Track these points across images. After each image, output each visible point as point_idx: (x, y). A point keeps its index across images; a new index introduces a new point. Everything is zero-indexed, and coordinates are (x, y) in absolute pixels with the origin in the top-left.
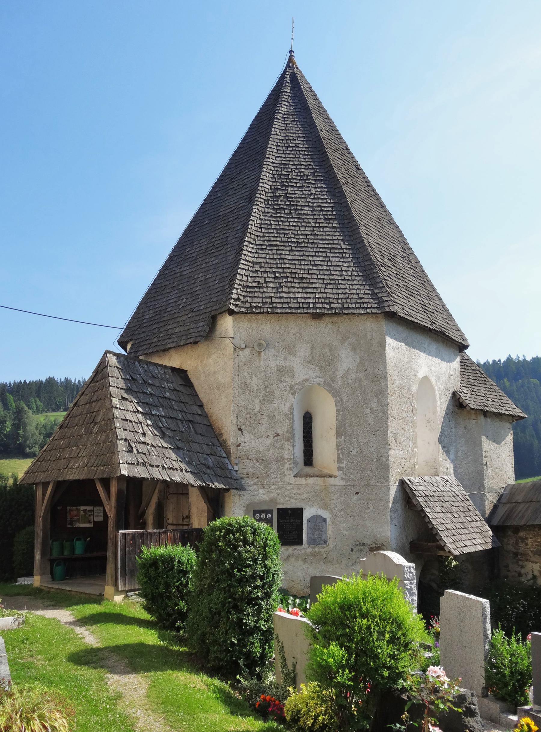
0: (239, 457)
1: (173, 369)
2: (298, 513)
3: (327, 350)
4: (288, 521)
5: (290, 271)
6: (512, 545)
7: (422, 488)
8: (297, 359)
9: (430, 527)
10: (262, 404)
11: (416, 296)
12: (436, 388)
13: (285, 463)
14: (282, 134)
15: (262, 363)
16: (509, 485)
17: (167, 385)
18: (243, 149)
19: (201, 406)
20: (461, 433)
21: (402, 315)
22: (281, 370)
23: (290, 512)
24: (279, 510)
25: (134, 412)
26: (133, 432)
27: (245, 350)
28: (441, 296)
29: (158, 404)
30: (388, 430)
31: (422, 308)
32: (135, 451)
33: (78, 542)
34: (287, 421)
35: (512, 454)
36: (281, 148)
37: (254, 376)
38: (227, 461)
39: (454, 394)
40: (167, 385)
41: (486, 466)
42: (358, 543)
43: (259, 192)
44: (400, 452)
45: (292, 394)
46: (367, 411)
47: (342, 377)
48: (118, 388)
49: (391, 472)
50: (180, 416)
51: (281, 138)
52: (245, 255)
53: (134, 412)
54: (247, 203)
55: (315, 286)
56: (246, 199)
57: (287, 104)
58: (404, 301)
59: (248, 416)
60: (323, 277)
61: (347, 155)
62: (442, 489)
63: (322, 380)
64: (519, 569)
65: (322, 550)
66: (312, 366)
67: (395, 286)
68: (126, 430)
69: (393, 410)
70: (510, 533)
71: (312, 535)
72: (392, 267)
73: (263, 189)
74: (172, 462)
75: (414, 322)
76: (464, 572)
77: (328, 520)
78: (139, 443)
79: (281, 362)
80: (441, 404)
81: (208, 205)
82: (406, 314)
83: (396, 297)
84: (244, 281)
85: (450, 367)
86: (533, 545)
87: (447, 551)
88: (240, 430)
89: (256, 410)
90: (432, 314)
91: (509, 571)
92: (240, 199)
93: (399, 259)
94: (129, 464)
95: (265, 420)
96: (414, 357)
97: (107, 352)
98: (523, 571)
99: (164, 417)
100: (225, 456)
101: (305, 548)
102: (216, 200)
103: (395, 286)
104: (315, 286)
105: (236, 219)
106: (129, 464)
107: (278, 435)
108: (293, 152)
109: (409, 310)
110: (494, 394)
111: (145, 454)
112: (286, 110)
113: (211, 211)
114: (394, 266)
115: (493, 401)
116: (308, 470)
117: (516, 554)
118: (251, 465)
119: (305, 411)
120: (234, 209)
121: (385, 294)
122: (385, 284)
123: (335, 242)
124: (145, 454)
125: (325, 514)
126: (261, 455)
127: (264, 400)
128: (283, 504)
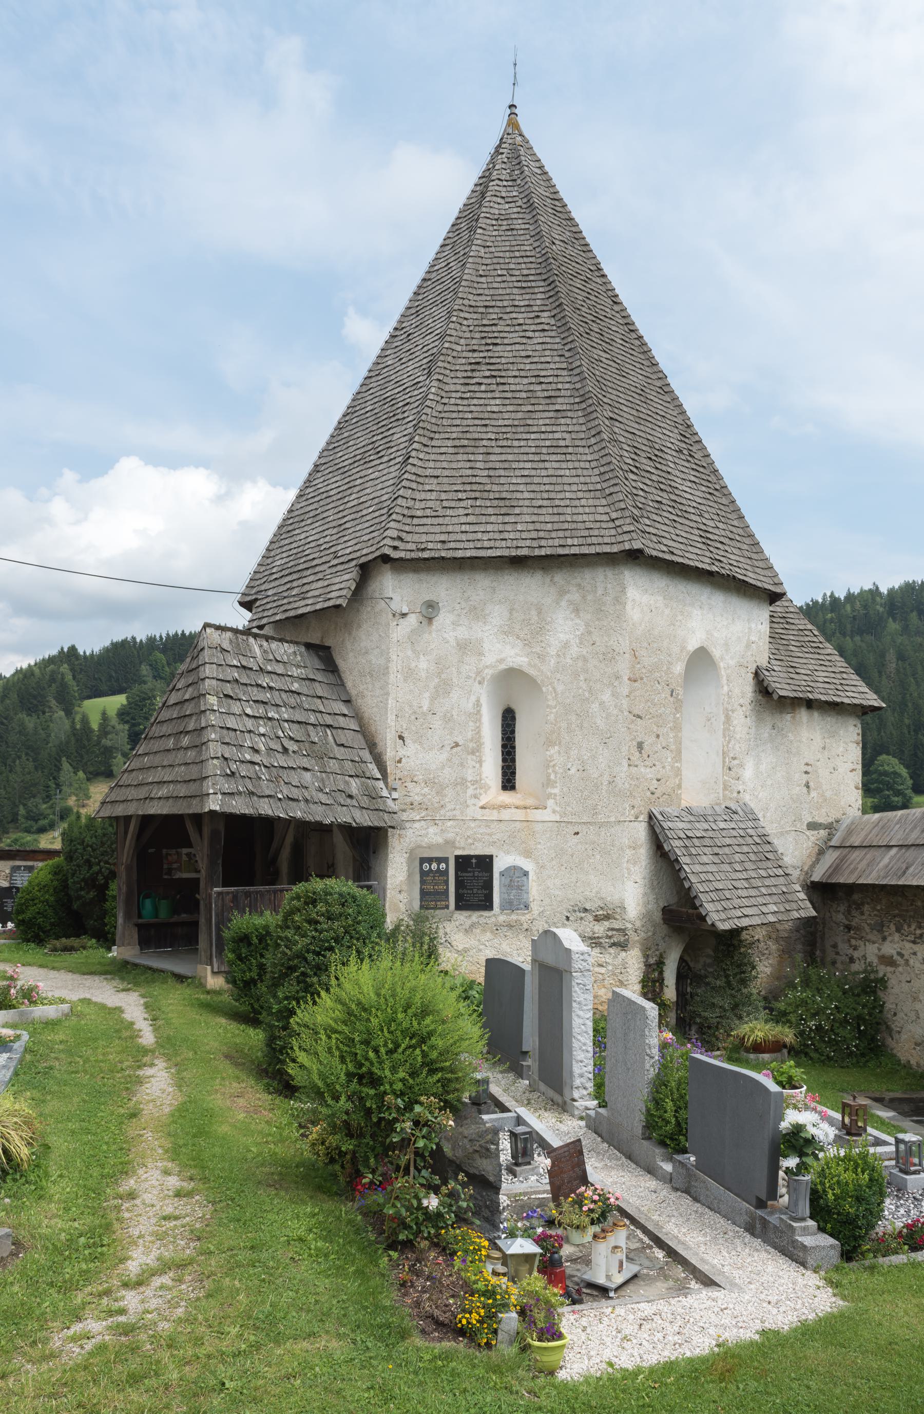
2: (486, 862)
7: (681, 825)
9: (687, 885)
10: (433, 699)
12: (722, 665)
13: (467, 787)
17: (295, 672)
20: (766, 735)
21: (654, 553)
22: (463, 646)
23: (474, 861)
28: (744, 511)
34: (471, 724)
35: (860, 767)
36: (483, 280)
38: (381, 784)
40: (295, 672)
41: (808, 787)
44: (648, 770)
45: (480, 683)
46: (595, 707)
50: (312, 720)
55: (517, 511)
57: (499, 200)
58: (664, 527)
59: (413, 717)
61: (598, 280)
62: (722, 825)
63: (526, 660)
65: (523, 918)
71: (506, 896)
72: (653, 470)
76: (763, 955)
77: (531, 875)
79: (462, 633)
81: (373, 379)
83: (648, 522)
85: (750, 628)
88: (401, 738)
89: (425, 709)
90: (719, 545)
91: (837, 953)
95: (437, 723)
96: (680, 618)
97: (206, 626)
99: (287, 721)
100: (379, 776)
101: (497, 914)
104: (517, 511)
107: (457, 745)
109: (671, 543)
110: (830, 669)
112: (497, 212)
116: (507, 797)
118: (418, 790)
123: (557, 436)
125: (527, 865)
128: (464, 848)
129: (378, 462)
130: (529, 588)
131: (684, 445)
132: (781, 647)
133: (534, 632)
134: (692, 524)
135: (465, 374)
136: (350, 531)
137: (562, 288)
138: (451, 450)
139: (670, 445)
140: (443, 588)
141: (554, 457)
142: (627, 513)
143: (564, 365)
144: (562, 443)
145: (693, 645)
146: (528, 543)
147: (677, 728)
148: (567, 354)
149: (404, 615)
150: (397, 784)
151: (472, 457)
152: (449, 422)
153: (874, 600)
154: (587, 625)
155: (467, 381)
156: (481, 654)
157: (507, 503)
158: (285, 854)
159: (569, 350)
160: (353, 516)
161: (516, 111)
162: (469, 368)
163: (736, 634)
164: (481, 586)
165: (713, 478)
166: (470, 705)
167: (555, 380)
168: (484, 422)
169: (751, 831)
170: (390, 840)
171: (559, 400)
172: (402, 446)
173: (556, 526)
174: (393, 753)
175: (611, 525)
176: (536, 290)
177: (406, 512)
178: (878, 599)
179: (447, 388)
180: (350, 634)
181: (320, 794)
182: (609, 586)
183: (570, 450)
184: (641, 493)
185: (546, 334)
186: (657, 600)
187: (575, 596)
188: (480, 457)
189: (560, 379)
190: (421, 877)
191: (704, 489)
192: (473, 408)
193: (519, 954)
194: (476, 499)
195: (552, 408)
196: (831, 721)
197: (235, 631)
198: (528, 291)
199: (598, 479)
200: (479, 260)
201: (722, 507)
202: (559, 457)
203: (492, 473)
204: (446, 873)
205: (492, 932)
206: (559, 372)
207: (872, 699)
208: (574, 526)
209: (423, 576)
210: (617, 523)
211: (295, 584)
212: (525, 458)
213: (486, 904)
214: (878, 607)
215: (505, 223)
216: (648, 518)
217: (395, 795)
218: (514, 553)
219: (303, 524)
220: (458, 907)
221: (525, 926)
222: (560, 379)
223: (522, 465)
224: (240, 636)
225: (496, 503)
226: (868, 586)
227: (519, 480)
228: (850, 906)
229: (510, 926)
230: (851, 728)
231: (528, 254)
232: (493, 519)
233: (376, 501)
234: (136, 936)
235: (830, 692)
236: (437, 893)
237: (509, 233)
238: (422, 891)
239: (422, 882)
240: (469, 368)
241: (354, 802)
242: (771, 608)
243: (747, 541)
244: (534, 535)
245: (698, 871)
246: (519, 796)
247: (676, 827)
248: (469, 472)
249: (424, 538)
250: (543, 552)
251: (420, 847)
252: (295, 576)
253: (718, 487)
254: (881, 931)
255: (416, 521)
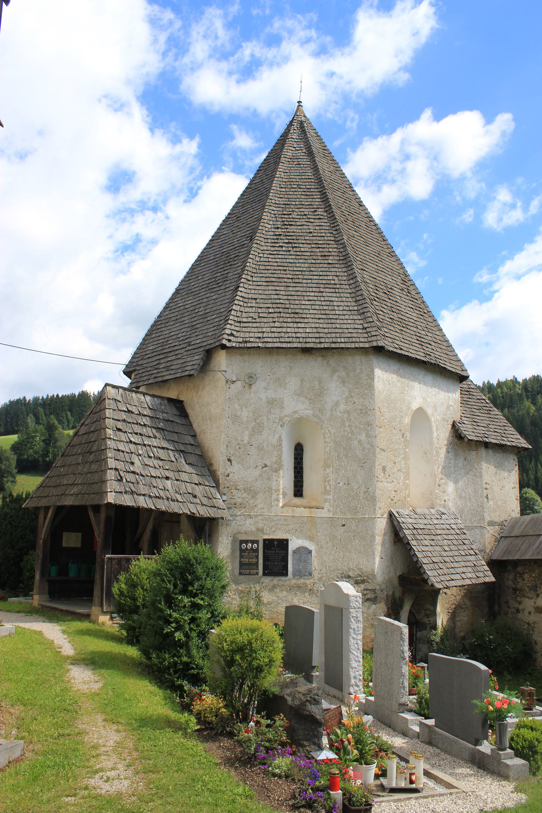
0: (228, 487)
1: (170, 400)
2: (283, 544)
3: (316, 383)
4: (274, 552)
5: (283, 306)
6: (512, 581)
8: (287, 391)
9: (415, 560)
10: (251, 436)
11: (412, 328)
12: (433, 419)
14: (285, 177)
15: (252, 395)
16: (512, 518)
18: (250, 190)
19: (194, 436)
20: (461, 464)
21: (391, 349)
22: (271, 402)
23: (276, 543)
24: (265, 540)
25: (127, 442)
26: (123, 461)
27: (237, 382)
29: (151, 435)
30: (375, 462)
31: (418, 340)
32: (124, 480)
33: (53, 567)
34: (275, 452)
36: (284, 190)
37: (244, 408)
39: (454, 425)
41: (487, 498)
42: (343, 576)
43: (259, 231)
44: (389, 484)
45: (281, 426)
47: (332, 410)
48: (113, 419)
49: (378, 505)
51: (284, 180)
52: (241, 291)
53: (127, 442)
54: (248, 241)
55: (306, 321)
56: (248, 237)
57: (292, 149)
59: (237, 447)
60: (314, 312)
61: (350, 193)
62: (436, 522)
63: (311, 412)
64: (517, 605)
65: (308, 582)
66: (302, 399)
67: (387, 319)
68: (118, 460)
69: (381, 442)
70: (510, 568)
72: (388, 300)
73: (264, 228)
74: (159, 490)
75: (405, 355)
78: (129, 472)
79: (271, 394)
80: (438, 435)
81: (215, 242)
82: (396, 348)
83: (386, 330)
84: (238, 317)
85: (449, 397)
86: (528, 580)
87: (430, 584)
88: (229, 460)
89: (245, 442)
90: (428, 346)
91: (509, 607)
92: (243, 237)
93: (397, 292)
94: (117, 492)
95: (253, 451)
96: (407, 389)
97: (107, 385)
98: (520, 607)
99: (155, 447)
101: (290, 579)
102: (222, 237)
103: (387, 319)
104: (306, 321)
105: (237, 256)
106: (117, 492)
107: (266, 466)
108: (295, 193)
109: (399, 343)
111: (133, 483)
112: (291, 155)
113: (216, 247)
114: (390, 299)
115: (495, 432)
116: (297, 500)
117: (515, 590)
118: (239, 495)
119: (297, 442)
120: (237, 247)
121: (375, 329)
122: (376, 318)
123: (329, 278)
124: (133, 483)
125: (311, 546)
126: (249, 486)
127: (253, 431)
129: (219, 289)
130: (313, 367)
131: (404, 286)
132: (467, 409)
133: (316, 395)
134: (412, 332)
135: (273, 241)
136: (200, 329)
137: (330, 196)
138: (264, 284)
139: (396, 286)
140: (258, 365)
141: (327, 290)
142: (373, 324)
143: (333, 239)
144: (333, 282)
145: (415, 406)
146: (313, 340)
147: (406, 458)
148: (334, 233)
149: (233, 382)
150: (226, 491)
151: (277, 288)
152: (264, 268)
153: (514, 386)
154: (350, 392)
155: (274, 245)
156: (282, 408)
157: (300, 316)
158: (147, 537)
159: (335, 230)
160: (201, 321)
161: (301, 104)
162: (275, 237)
163: (440, 402)
164: (282, 366)
165: (422, 306)
166: (275, 440)
167: (328, 246)
168: (285, 268)
169: (454, 526)
170: (220, 527)
171: (331, 258)
172: (233, 281)
173: (330, 331)
174: (224, 470)
175: (364, 331)
176: (315, 197)
177: (236, 319)
178: (517, 385)
179: (262, 248)
180: (197, 393)
181: (177, 495)
182: (363, 368)
183: (338, 286)
184: (381, 313)
185: (322, 221)
186: (393, 377)
187: (343, 374)
188: (283, 288)
189: (331, 246)
190: (240, 553)
191: (417, 312)
192: (278, 260)
193: (313, 605)
194: (280, 312)
195: (326, 262)
196: (499, 456)
197: (124, 389)
198: (310, 197)
199: (353, 304)
200: (281, 179)
201: (429, 323)
202: (331, 290)
203: (289, 297)
204: (257, 550)
205: (287, 591)
206: (330, 242)
207: (523, 443)
208: (341, 331)
209: (246, 357)
210: (368, 330)
211: (162, 361)
212: (311, 289)
213: (284, 572)
214: (517, 390)
215: (296, 160)
216: (386, 328)
217: (225, 498)
218: (304, 346)
219: (168, 324)
220: (265, 574)
221: (309, 587)
222: (331, 246)
223: (308, 294)
224: (127, 392)
225: (292, 315)
226: (510, 378)
227: (307, 303)
228: (516, 575)
229: (299, 587)
230: (512, 461)
231: (310, 177)
232: (291, 325)
233: (217, 312)
234: (47, 589)
235: (499, 438)
236: (250, 564)
237: (299, 166)
238: (240, 562)
239: (241, 557)
240: (275, 237)
241: (198, 501)
242: (461, 386)
243: (444, 344)
244: (317, 335)
245: (422, 550)
246: (305, 500)
247: (406, 521)
248: (276, 297)
249: (247, 335)
250: (322, 346)
251: (239, 533)
252: (162, 356)
253: (426, 312)
254: (535, 590)
255: (242, 325)
